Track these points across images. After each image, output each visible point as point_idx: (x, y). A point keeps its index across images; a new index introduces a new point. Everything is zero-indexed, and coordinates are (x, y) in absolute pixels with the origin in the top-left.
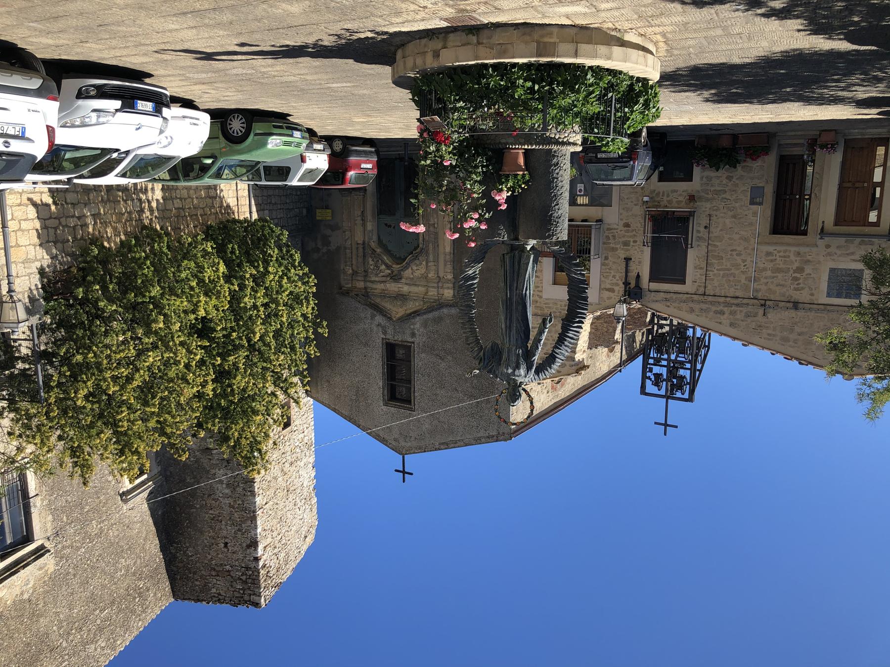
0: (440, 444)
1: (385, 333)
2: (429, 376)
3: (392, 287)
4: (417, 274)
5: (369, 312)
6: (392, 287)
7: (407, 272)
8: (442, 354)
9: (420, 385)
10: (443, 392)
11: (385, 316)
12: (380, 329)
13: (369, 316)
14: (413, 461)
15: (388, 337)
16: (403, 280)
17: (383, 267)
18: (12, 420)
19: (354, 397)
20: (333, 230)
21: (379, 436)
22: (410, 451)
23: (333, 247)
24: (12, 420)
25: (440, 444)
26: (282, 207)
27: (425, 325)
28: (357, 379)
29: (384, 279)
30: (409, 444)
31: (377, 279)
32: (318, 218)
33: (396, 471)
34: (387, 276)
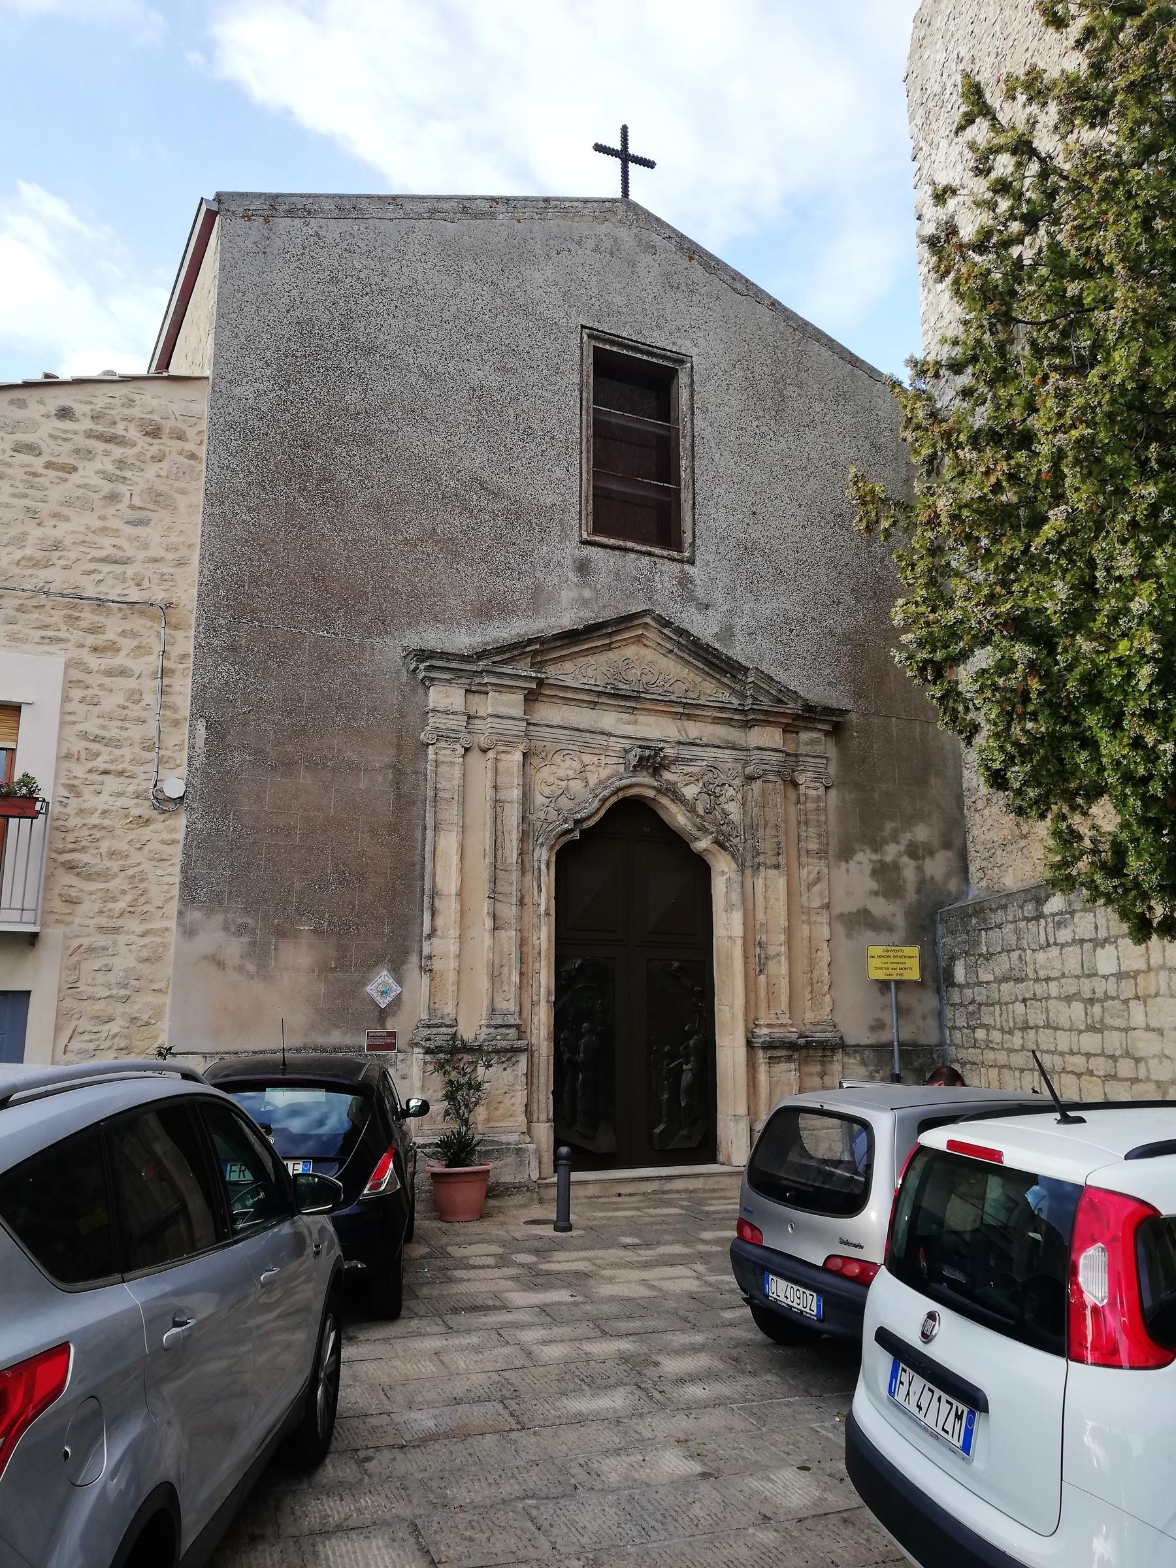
0: (493, 216)
1: (685, 581)
2: (528, 433)
3: (655, 728)
4: (565, 766)
5: (738, 652)
6: (655, 728)
7: (604, 773)
8: (476, 499)
9: (563, 401)
10: (480, 374)
11: (681, 632)
12: (700, 593)
13: (740, 636)
14: (601, 180)
15: (676, 567)
16: (616, 744)
17: (690, 792)
18: (997, 286)
19: (789, 391)
20: (865, 912)
21: (707, 267)
22: (601, 208)
23: (864, 858)
24: (997, 286)
25: (493, 216)
26: (1040, 989)
27: (538, 599)
28: (782, 444)
29: (686, 752)
30: (602, 229)
31: (711, 753)
32: (914, 950)
33: (599, 148)
34: (676, 760)
